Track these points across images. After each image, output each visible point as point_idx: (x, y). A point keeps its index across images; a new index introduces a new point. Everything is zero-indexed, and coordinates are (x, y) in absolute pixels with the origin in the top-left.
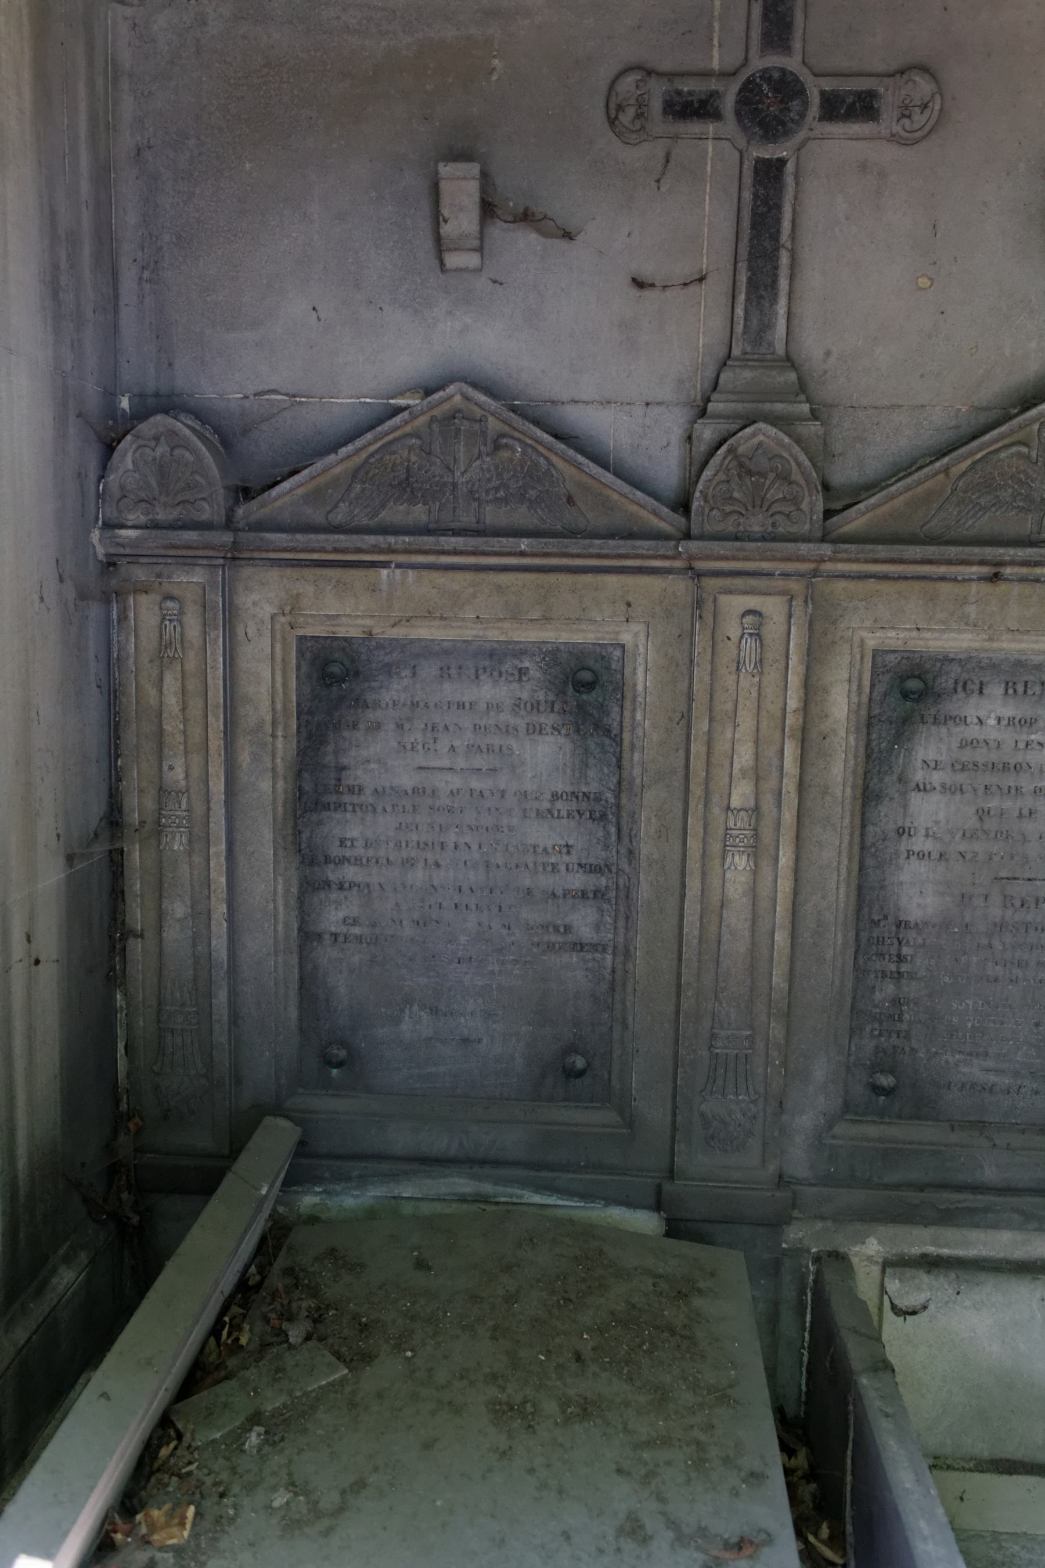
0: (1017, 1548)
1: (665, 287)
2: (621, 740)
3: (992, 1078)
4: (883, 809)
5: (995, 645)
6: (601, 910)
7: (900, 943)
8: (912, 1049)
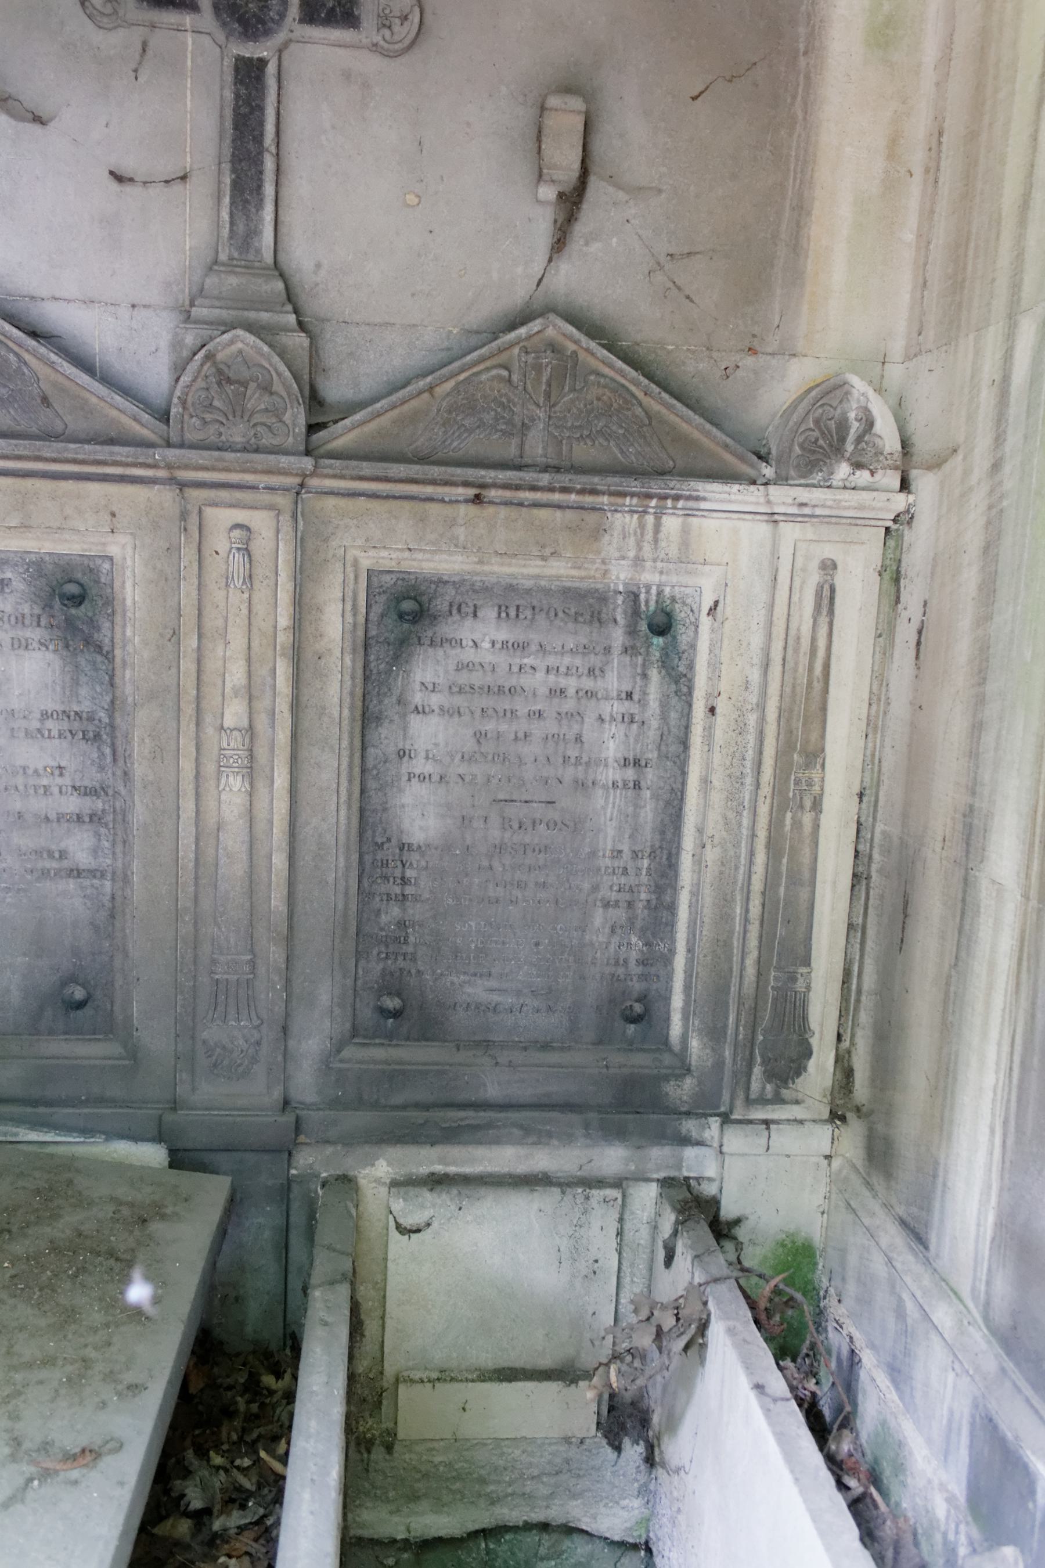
0: (517, 1452)
1: (145, 183)
2: (114, 657)
3: (495, 998)
4: (384, 731)
5: (486, 568)
6: (98, 835)
7: (404, 866)
8: (419, 971)
